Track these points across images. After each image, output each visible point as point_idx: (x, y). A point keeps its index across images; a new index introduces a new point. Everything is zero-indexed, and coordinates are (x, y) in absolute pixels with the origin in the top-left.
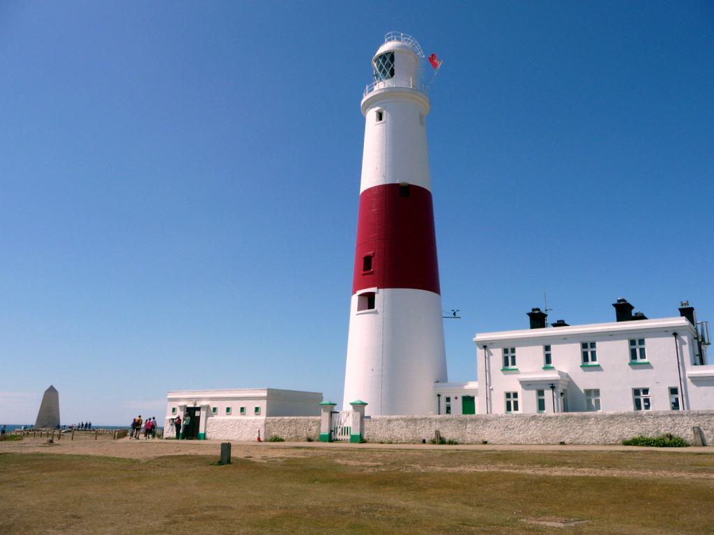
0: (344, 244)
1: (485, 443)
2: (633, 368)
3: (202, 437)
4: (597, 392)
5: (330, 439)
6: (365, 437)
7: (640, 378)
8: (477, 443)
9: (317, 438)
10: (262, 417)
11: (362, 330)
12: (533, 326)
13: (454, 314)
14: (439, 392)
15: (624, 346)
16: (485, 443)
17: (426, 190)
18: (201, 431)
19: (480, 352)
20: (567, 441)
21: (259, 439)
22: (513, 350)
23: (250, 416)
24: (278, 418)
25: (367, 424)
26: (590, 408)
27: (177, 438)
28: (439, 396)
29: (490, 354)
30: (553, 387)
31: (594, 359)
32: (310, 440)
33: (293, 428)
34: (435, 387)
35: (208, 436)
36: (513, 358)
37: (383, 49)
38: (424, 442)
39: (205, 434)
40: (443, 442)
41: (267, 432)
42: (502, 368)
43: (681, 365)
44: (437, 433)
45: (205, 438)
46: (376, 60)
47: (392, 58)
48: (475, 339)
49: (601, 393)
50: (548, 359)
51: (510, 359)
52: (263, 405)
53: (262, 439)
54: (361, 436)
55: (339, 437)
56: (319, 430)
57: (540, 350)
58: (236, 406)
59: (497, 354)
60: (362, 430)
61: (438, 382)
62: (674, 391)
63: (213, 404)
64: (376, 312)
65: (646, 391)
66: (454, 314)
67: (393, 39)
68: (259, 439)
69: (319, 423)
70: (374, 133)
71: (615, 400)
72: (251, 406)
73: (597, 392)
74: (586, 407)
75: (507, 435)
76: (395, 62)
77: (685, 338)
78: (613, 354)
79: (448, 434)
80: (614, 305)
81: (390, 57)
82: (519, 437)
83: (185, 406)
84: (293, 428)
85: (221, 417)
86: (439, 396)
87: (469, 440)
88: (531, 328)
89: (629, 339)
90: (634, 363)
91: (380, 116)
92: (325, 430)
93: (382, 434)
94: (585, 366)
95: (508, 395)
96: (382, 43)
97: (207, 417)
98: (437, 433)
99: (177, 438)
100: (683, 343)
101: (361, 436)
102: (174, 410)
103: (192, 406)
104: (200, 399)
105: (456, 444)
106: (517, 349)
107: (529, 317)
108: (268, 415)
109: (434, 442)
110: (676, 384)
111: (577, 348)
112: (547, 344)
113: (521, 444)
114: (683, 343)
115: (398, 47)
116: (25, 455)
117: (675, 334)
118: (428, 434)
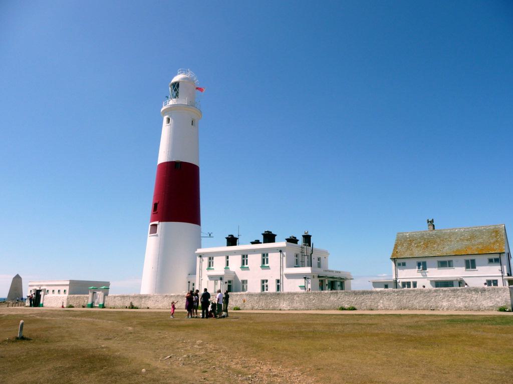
0: (146, 192)
1: (148, 308)
2: (242, 270)
3: (41, 305)
4: (247, 281)
5: (92, 306)
6: (105, 305)
7: (265, 275)
8: (145, 308)
9: (87, 306)
10: (67, 295)
11: (152, 243)
12: (228, 245)
13: (210, 235)
14: (189, 280)
15: (259, 257)
16: (148, 308)
17: (182, 163)
18: (41, 303)
19: (198, 259)
20: (150, 307)
21: (63, 307)
22: (267, 255)
23: (62, 295)
24: (73, 295)
25: (107, 299)
26: (243, 290)
27: (31, 306)
28: (189, 282)
29: (203, 260)
30: (221, 279)
31: (267, 263)
32: (84, 307)
33: (78, 301)
34: (188, 277)
35: (44, 305)
36: (267, 259)
37: (176, 79)
38: (126, 308)
39: (42, 304)
40: (132, 307)
41: (68, 303)
42: (261, 266)
43: (281, 267)
44: (131, 303)
45: (42, 306)
46: (171, 86)
47: (178, 84)
48: (196, 252)
49: (248, 282)
50: (228, 265)
51: (266, 260)
52: (67, 288)
53: (65, 306)
54: (103, 305)
55: (96, 305)
56: (87, 302)
57: (224, 258)
58: (56, 289)
59: (206, 260)
60: (104, 301)
61: (189, 275)
62: (278, 281)
63: (47, 288)
64: (157, 236)
65: (267, 281)
66: (210, 235)
67: (183, 73)
68: (63, 307)
69: (88, 298)
70: (166, 130)
71: (254, 287)
72: (62, 289)
73: (247, 281)
74: (241, 289)
75: (156, 305)
76: (179, 88)
77: (285, 253)
78: (255, 260)
79: (135, 304)
80: (263, 234)
81: (176, 86)
82: (160, 306)
83: (35, 289)
84: (78, 301)
85: (50, 295)
86: (189, 282)
87: (142, 307)
88: (227, 246)
89: (262, 253)
90: (263, 267)
91: (169, 120)
92: (90, 303)
93: (111, 304)
94: (243, 268)
95: (263, 281)
96: (176, 74)
97: (44, 295)
98: (131, 303)
99: (31, 306)
100: (284, 256)
101: (103, 305)
102: (31, 291)
103: (39, 289)
104: (42, 285)
105: (137, 308)
106: (269, 254)
107: (263, 236)
108: (70, 294)
109: (129, 308)
110: (279, 278)
111: (240, 257)
112: (227, 255)
113: (285, 310)
114: (284, 256)
115: (182, 79)
116: (13, 315)
117: (281, 251)
118: (128, 304)
